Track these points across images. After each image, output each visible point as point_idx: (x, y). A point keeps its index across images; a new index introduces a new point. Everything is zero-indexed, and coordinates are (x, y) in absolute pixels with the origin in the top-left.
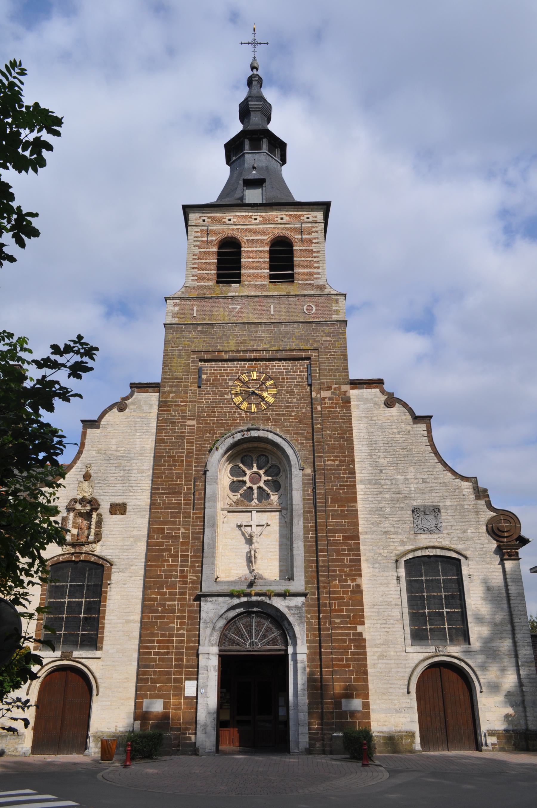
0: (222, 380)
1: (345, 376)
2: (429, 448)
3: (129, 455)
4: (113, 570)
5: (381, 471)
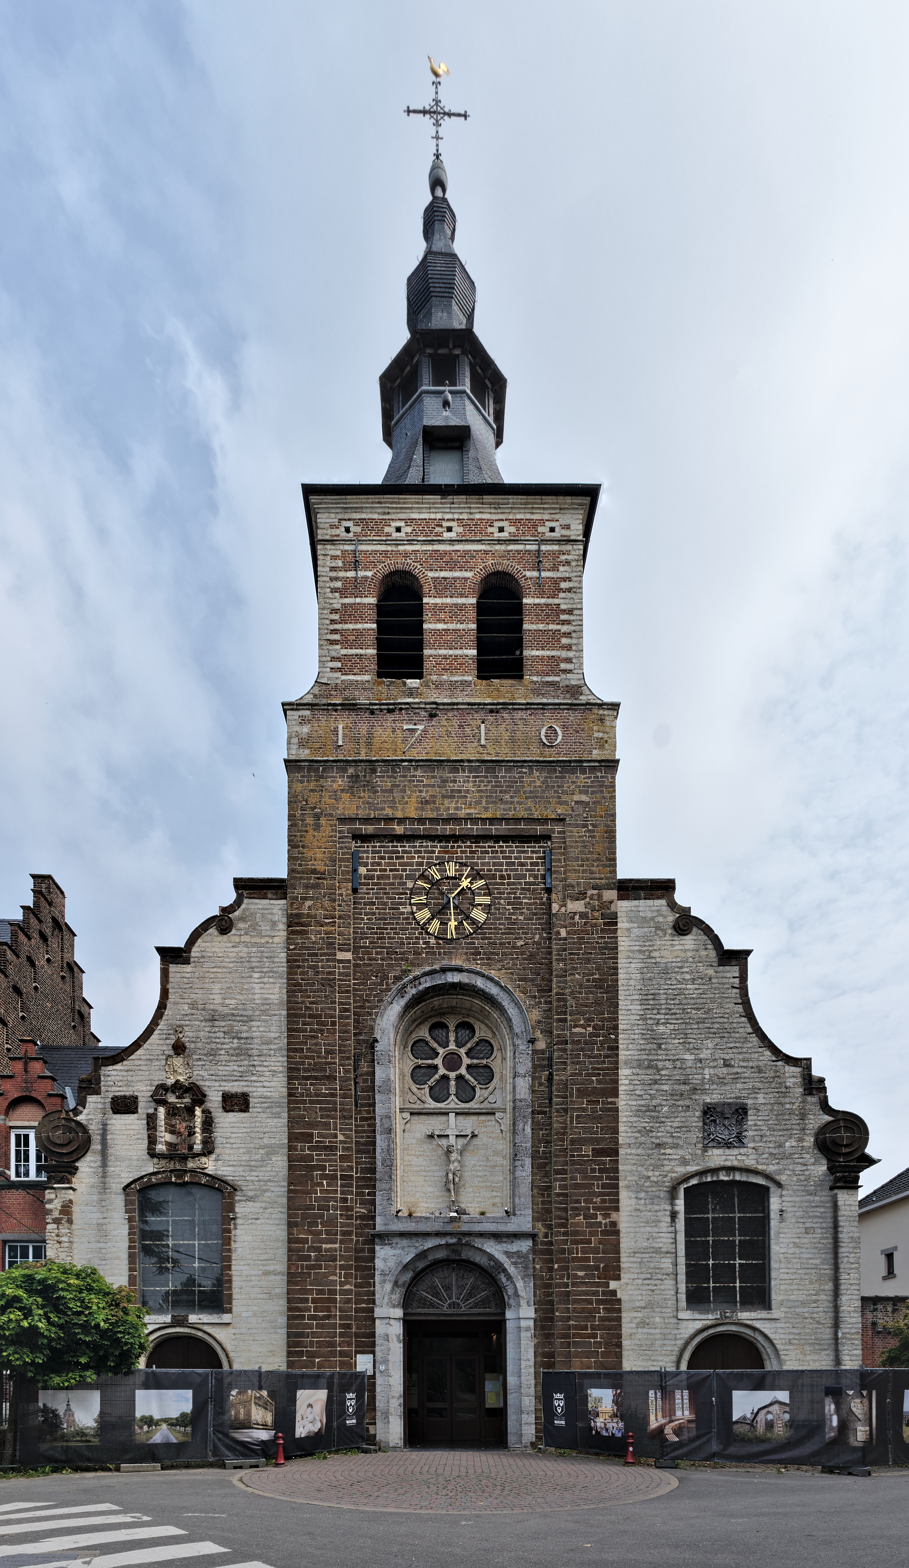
0: (395, 877)
1: (610, 872)
2: (740, 1008)
3: (244, 1013)
4: (237, 1198)
5: (659, 1046)
